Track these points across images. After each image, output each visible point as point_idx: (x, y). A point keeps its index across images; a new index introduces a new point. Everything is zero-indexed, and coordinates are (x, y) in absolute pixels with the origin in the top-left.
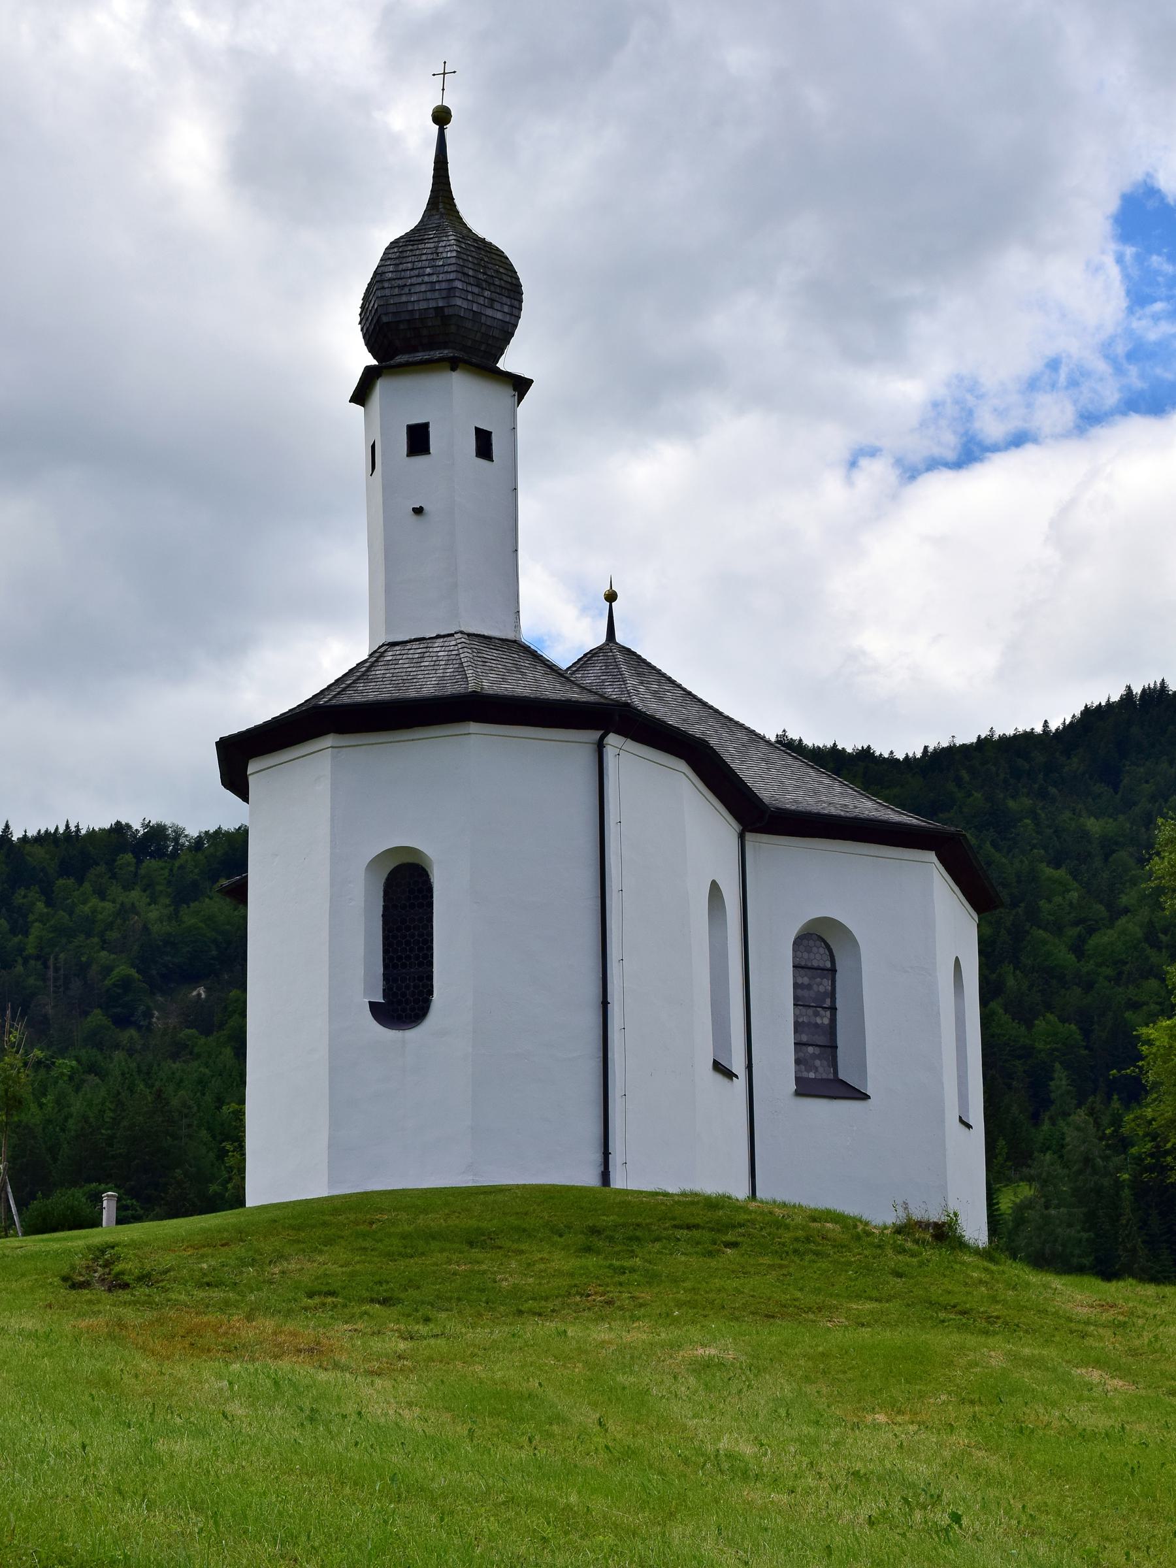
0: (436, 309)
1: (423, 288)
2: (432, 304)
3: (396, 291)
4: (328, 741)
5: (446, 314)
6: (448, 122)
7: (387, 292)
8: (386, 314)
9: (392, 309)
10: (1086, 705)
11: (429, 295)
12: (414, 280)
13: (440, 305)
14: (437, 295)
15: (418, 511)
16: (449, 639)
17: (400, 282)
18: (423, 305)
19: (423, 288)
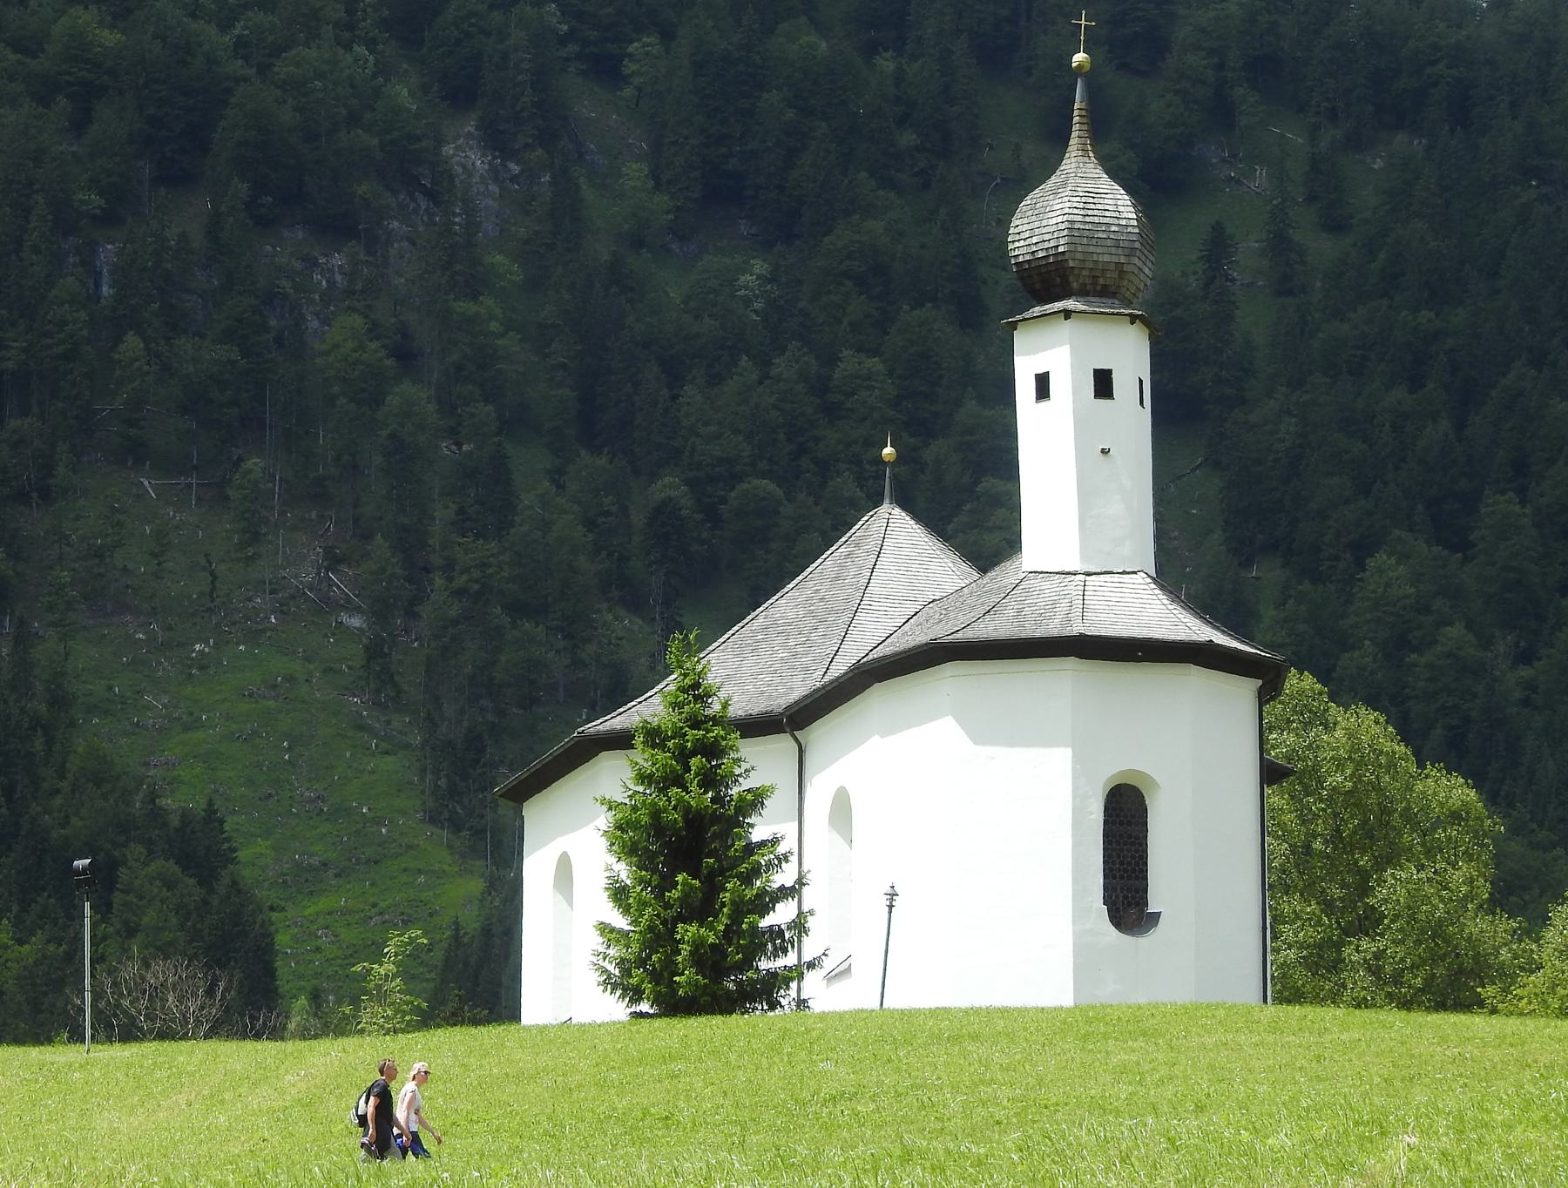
3: (1085, 241)
5: (1125, 270)
9: (1079, 256)
10: (786, 955)
11: (1113, 250)
14: (1120, 251)
15: (1105, 452)
16: (1134, 576)
18: (1106, 258)
19: (1109, 243)
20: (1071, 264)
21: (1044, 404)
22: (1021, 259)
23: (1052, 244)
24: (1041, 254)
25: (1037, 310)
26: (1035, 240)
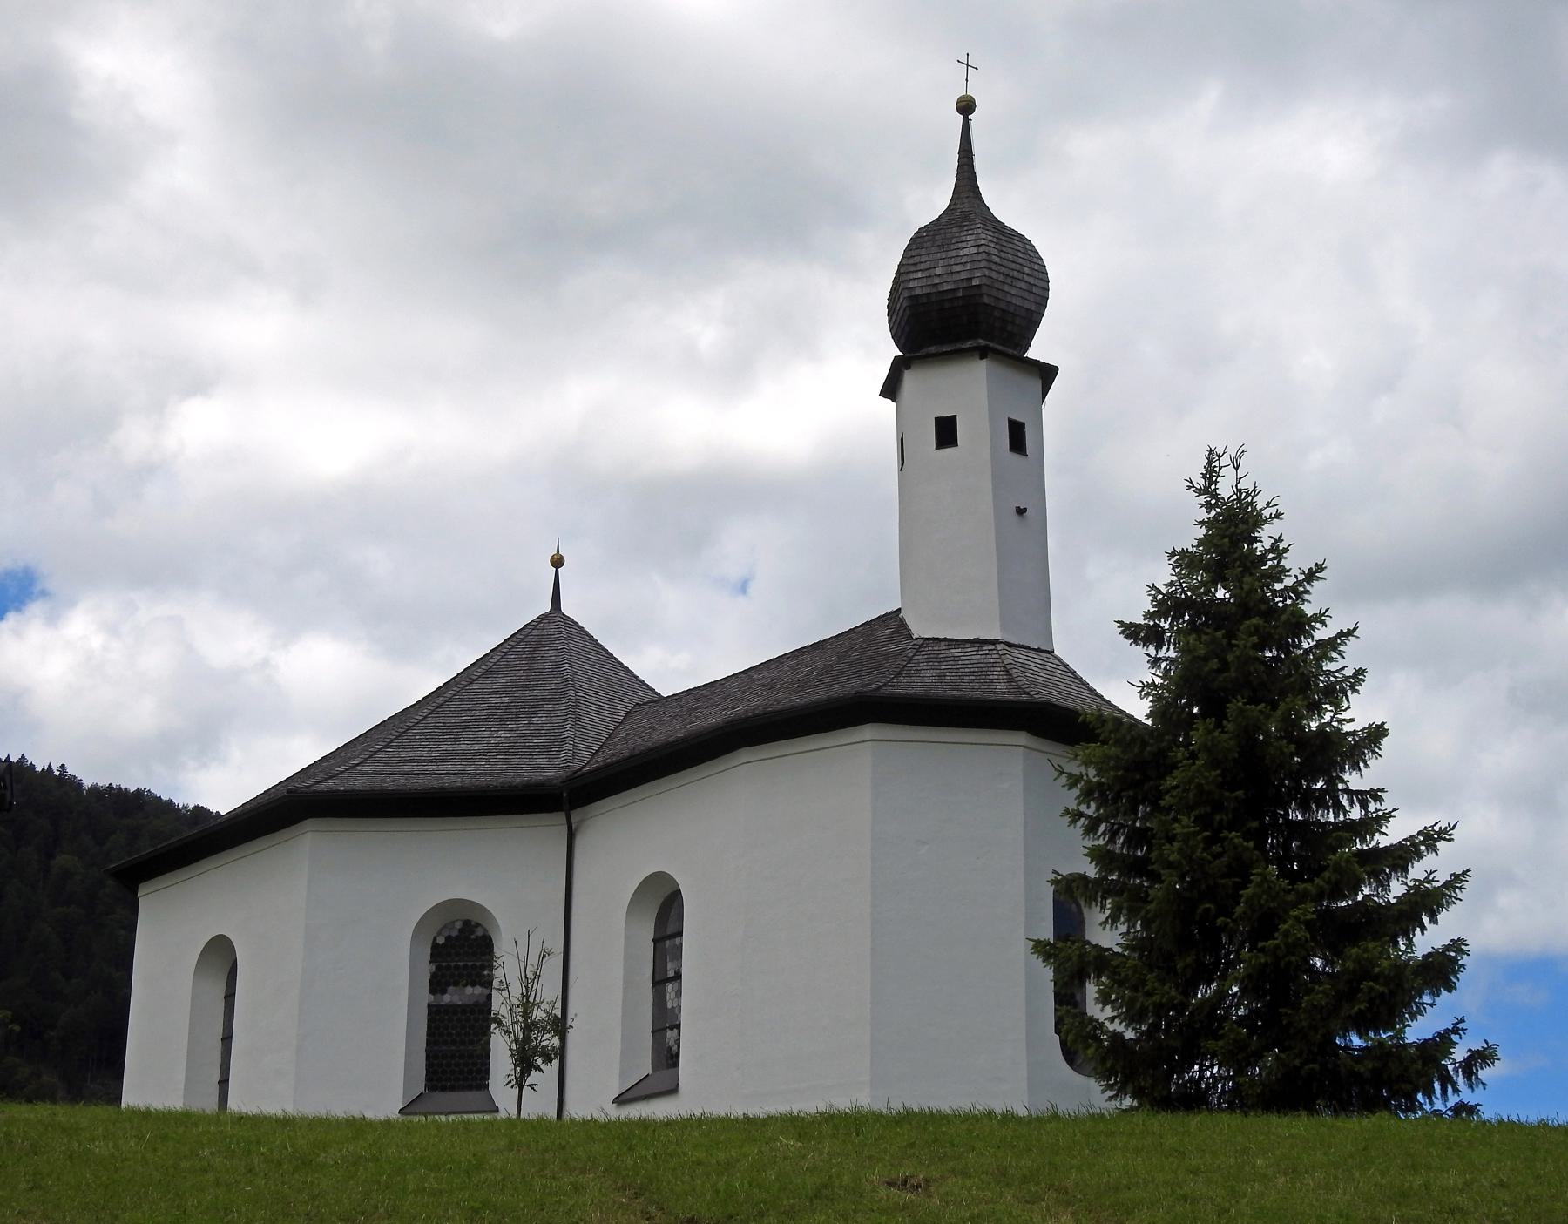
0: (1027, 309)
1: (1023, 285)
2: (1027, 305)
3: (1001, 278)
4: (1022, 738)
6: (972, 111)
7: (994, 275)
8: (989, 296)
9: (994, 293)
12: (1016, 274)
13: (1033, 309)
14: (1032, 297)
15: (1021, 512)
17: (1002, 269)
18: (1019, 302)
20: (986, 300)
21: (948, 452)
22: (918, 292)
23: (964, 276)
24: (946, 287)
25: (932, 349)
26: (938, 271)
